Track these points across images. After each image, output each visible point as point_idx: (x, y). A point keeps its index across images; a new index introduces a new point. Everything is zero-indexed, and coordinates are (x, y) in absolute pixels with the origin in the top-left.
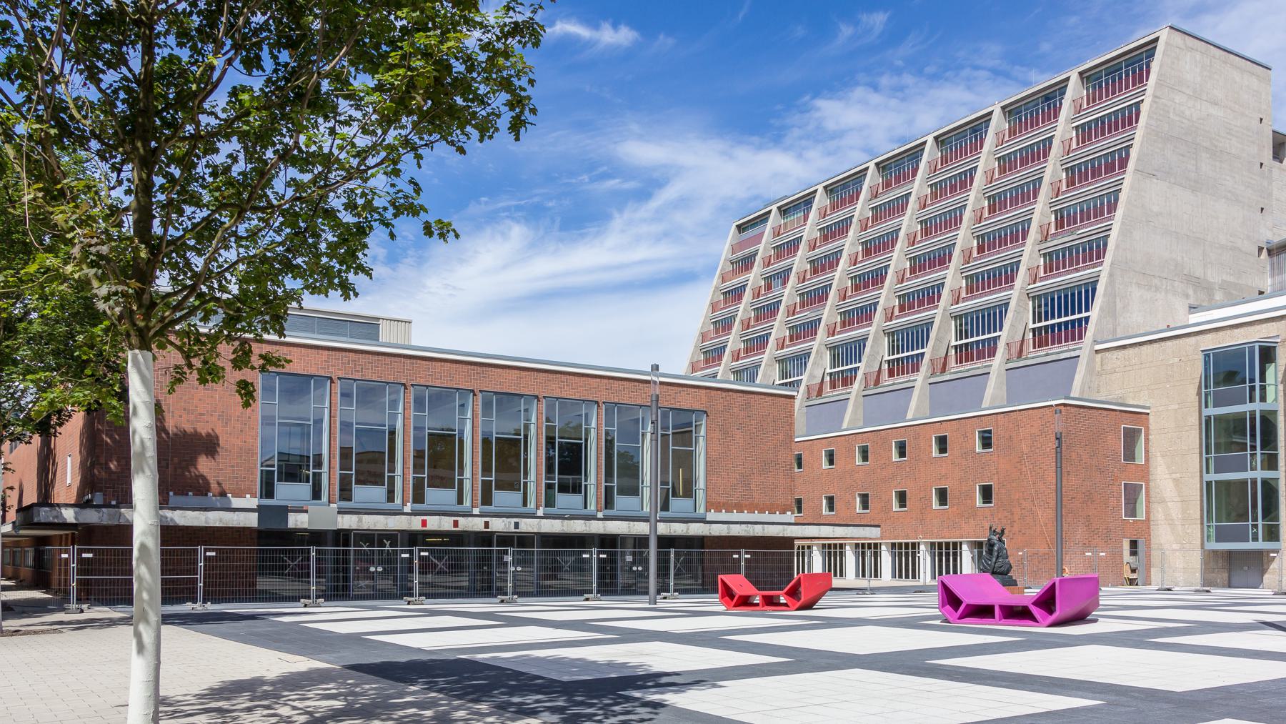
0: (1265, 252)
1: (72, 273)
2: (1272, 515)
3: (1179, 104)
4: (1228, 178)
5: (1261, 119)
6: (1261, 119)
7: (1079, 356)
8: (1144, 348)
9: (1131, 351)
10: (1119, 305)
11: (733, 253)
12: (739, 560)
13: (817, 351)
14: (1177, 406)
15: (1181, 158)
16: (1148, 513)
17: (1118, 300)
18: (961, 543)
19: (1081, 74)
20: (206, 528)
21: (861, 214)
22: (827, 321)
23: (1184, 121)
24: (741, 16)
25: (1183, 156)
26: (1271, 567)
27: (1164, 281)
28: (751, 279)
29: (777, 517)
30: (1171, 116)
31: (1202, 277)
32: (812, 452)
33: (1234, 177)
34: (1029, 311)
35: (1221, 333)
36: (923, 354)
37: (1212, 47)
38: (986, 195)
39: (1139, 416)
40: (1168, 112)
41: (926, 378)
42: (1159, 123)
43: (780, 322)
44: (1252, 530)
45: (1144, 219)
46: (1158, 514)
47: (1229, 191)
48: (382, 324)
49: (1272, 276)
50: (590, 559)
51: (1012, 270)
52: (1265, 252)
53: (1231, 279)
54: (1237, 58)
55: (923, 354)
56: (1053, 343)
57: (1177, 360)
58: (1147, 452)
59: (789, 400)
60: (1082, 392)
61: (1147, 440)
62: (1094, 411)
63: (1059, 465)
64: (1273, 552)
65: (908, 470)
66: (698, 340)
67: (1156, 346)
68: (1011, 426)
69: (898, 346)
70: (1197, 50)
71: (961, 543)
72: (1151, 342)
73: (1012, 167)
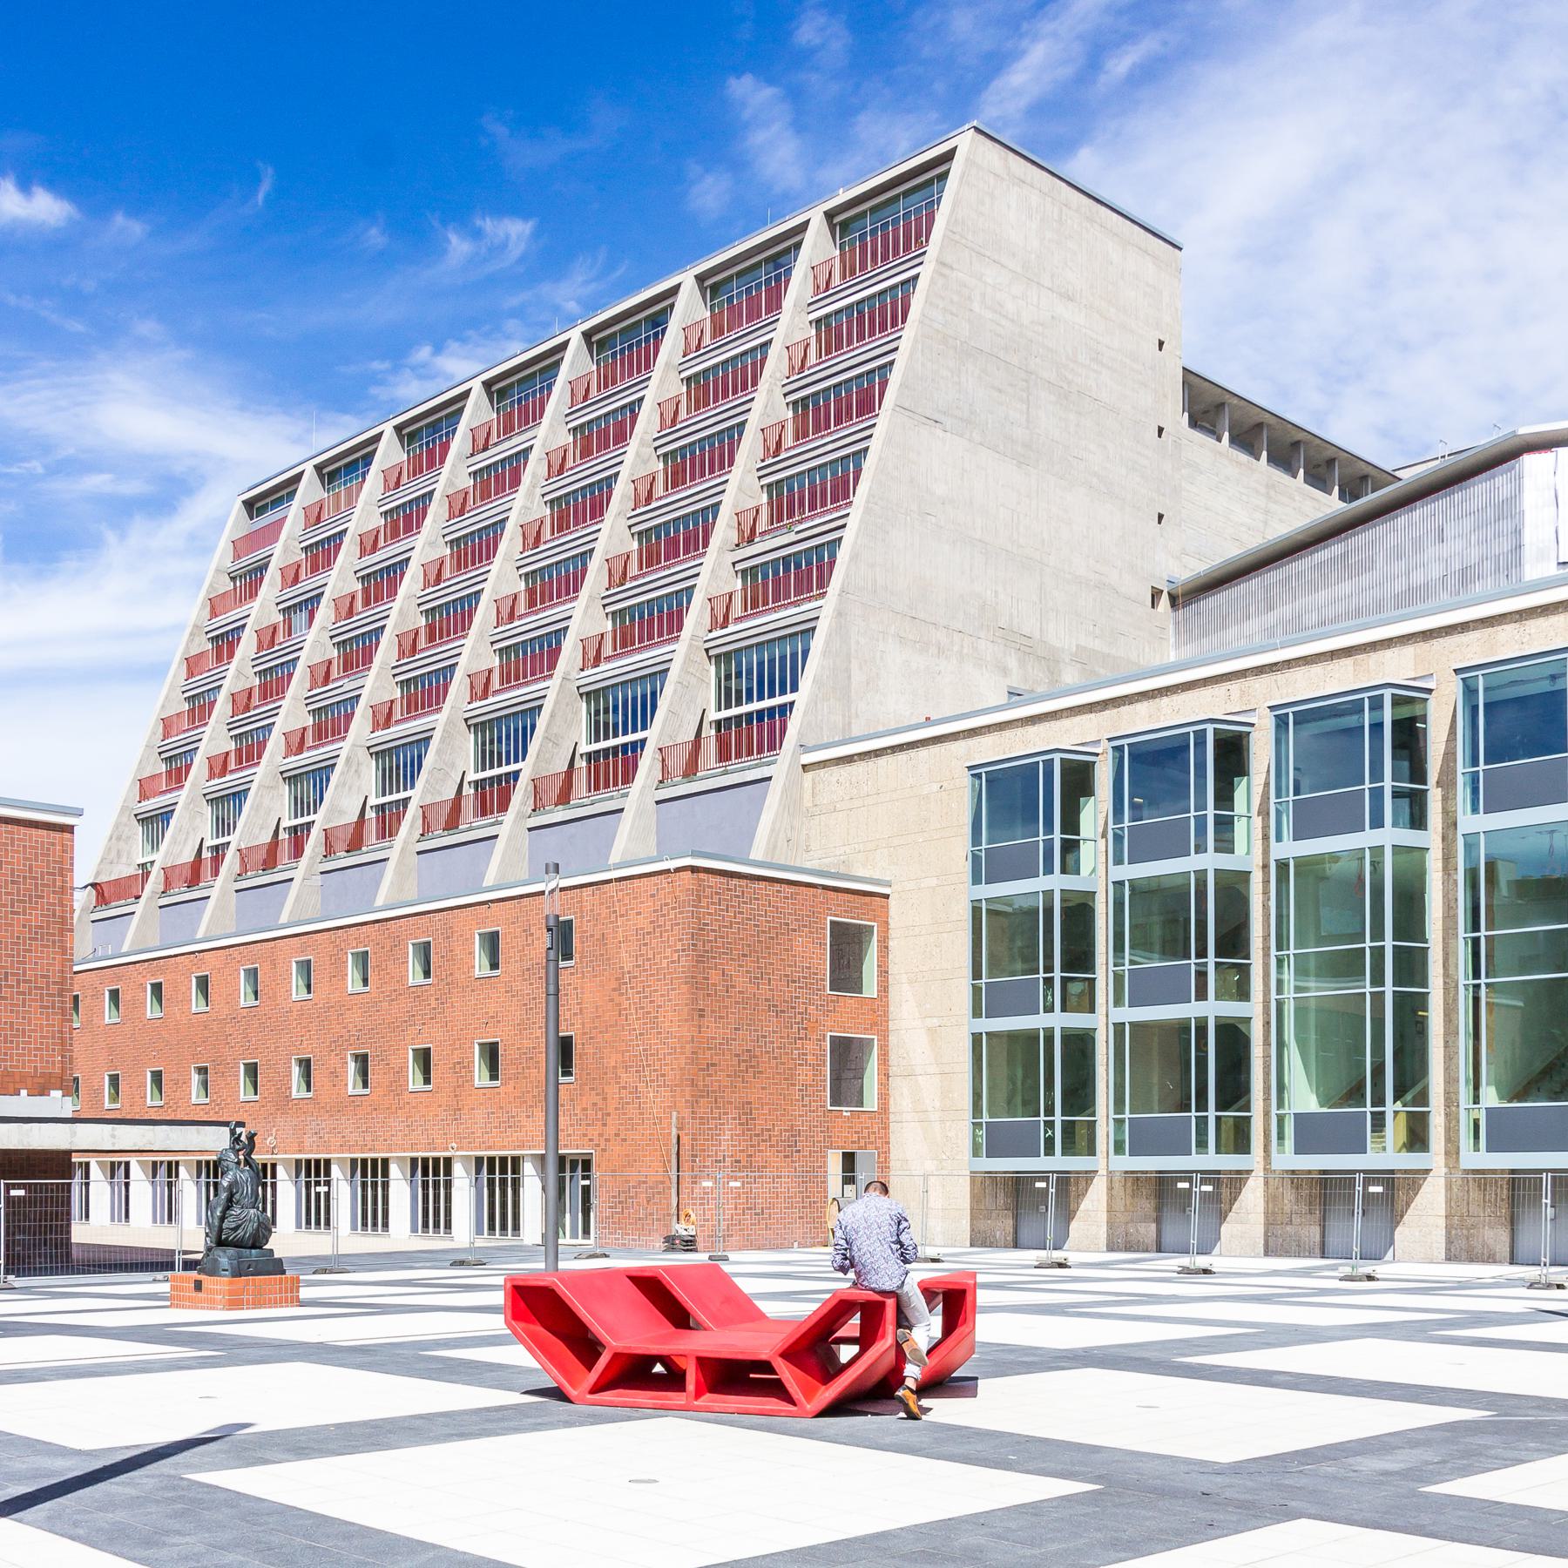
0: (1164, 600)
2: (1242, 1102)
5: (1161, 344)
6: (1161, 344)
7: (769, 779)
8: (882, 761)
9: (859, 768)
10: (857, 677)
11: (237, 556)
13: (348, 760)
14: (933, 882)
16: (884, 1097)
17: (854, 665)
18: (177, 1163)
19: (829, 215)
21: (450, 483)
22: (369, 700)
23: (1003, 322)
25: (1000, 391)
26: (1082, 1207)
27: (957, 637)
28: (254, 613)
30: (976, 307)
31: (1037, 635)
32: (274, 964)
34: (708, 684)
35: (1007, 733)
36: (516, 774)
37: (1064, 185)
38: (660, 451)
41: (520, 816)
43: (294, 698)
44: (1046, 1132)
46: (901, 1100)
49: (1178, 646)
51: (680, 604)
52: (1165, 598)
53: (1097, 645)
54: (1115, 215)
55: (516, 774)
56: (738, 755)
57: (936, 787)
58: (884, 972)
59: (58, 835)
60: (772, 847)
61: (884, 948)
62: (762, 885)
63: (552, 989)
64: (1041, 1179)
65: (433, 1003)
66: (154, 733)
67: (902, 757)
68: (605, 912)
69: (500, 754)
71: (177, 1163)
72: (895, 749)
73: (821, 425)
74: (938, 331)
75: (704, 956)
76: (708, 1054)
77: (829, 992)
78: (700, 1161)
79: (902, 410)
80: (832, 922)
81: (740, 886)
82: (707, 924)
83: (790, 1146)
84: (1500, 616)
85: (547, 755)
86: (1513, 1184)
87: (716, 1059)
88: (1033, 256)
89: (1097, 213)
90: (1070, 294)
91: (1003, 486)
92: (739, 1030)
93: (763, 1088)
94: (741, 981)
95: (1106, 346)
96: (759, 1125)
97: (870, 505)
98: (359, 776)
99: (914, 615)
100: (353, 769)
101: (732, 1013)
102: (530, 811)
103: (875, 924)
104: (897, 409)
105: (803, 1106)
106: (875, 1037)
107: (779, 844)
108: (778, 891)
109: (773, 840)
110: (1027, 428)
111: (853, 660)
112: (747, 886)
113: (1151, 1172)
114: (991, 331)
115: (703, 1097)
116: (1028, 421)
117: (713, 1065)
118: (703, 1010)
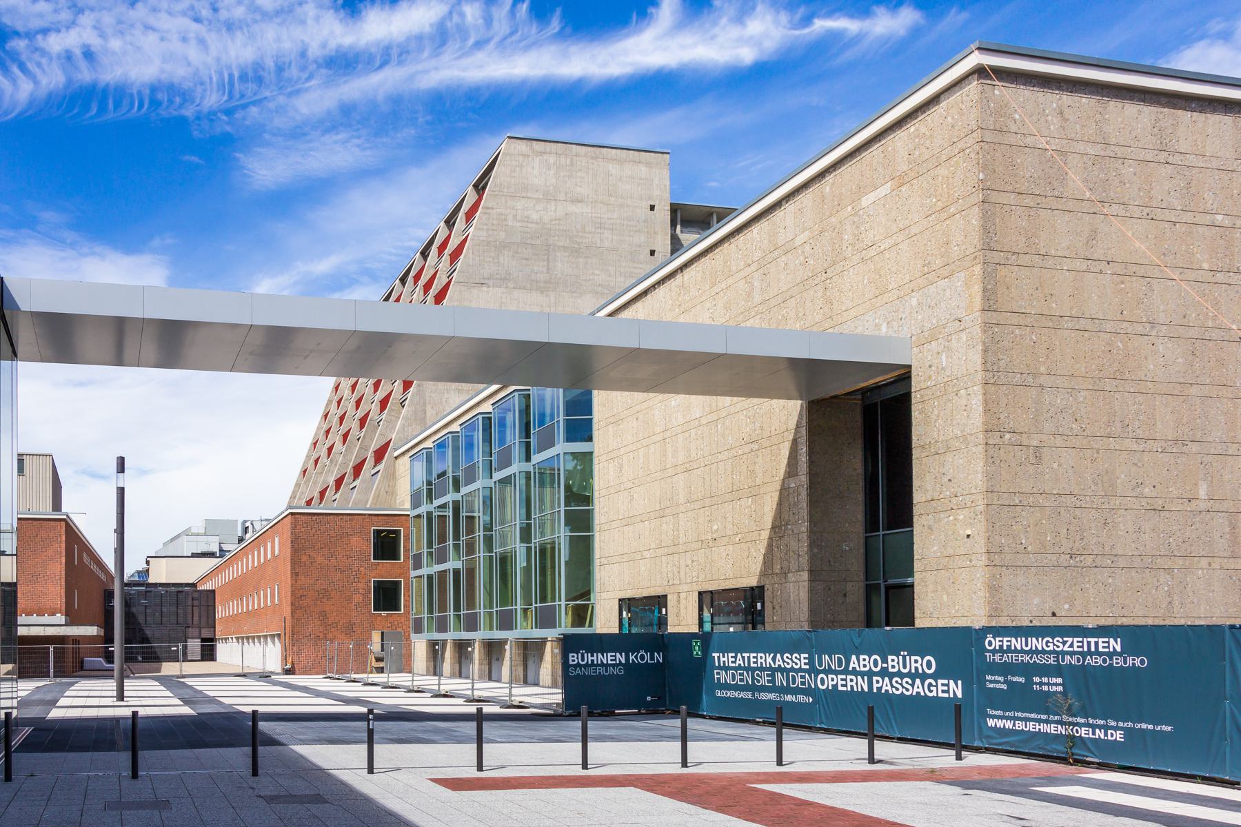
1: (931, 384)
4: (597, 272)
12: (178, 651)
15: (524, 262)
17: (428, 408)
20: (28, 636)
25: (527, 259)
29: (46, 619)
39: (397, 518)
40: (506, 220)
42: (491, 232)
48: (119, 486)
50: (178, 651)
70: (550, 153)
74: (483, 241)
83: (349, 630)
87: (305, 593)
90: (579, 199)
94: (320, 559)
95: (608, 219)
107: (382, 493)
109: (377, 493)
116: (548, 269)
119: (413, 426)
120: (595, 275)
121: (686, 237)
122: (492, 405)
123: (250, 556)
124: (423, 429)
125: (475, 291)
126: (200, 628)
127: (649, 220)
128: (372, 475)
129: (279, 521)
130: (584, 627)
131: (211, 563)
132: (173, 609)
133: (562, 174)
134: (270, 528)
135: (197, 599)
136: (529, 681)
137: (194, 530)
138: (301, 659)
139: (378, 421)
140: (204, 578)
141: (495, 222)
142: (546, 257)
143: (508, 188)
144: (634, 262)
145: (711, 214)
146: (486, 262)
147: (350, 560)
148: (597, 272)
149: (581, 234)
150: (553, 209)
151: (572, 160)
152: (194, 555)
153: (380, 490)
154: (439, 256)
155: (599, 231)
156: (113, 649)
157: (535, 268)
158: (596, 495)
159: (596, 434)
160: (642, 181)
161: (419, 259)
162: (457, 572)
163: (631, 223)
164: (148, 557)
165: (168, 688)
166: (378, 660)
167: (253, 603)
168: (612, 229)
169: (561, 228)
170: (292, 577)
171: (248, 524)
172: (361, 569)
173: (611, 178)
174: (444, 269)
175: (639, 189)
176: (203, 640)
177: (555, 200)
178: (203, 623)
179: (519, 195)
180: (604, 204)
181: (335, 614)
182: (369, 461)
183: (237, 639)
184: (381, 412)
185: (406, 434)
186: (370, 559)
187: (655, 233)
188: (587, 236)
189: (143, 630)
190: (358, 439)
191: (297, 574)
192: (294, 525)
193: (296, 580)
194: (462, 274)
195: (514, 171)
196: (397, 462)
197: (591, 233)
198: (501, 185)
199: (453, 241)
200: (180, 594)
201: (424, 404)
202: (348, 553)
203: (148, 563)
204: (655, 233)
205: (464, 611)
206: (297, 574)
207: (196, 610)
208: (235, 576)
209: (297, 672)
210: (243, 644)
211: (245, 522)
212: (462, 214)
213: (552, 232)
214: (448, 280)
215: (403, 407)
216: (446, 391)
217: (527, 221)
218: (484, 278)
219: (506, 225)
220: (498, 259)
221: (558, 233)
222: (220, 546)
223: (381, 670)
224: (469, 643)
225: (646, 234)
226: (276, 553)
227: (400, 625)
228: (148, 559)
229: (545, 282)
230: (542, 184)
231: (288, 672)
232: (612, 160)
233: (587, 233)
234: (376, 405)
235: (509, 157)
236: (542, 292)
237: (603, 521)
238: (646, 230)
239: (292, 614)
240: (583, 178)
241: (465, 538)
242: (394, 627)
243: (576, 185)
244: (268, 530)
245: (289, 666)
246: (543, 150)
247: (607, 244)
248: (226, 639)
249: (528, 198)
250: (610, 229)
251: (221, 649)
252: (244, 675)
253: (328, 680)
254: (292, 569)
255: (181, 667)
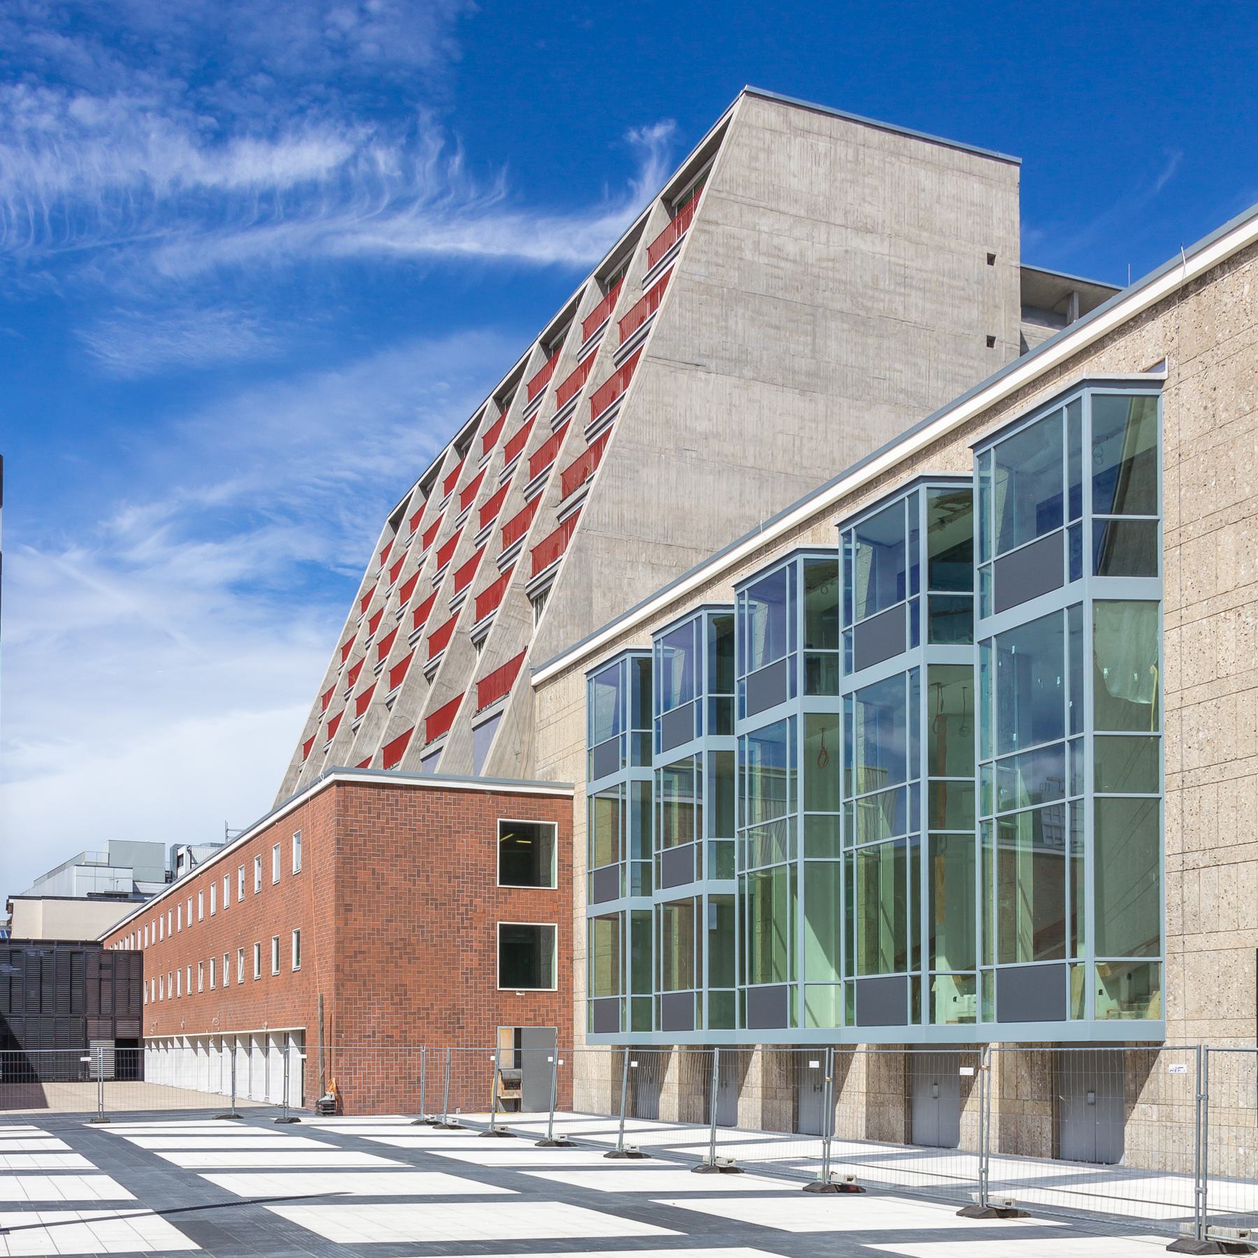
3: (770, 234)
4: (898, 366)
15: (772, 332)
17: (597, 595)
24: (1161, 183)
25: (777, 328)
30: (748, 255)
33: (915, 365)
39: (547, 801)
40: (740, 248)
42: (713, 269)
45: (671, 446)
47: (902, 391)
62: (419, 793)
70: (819, 134)
74: (700, 283)
75: (351, 858)
76: (355, 944)
77: (498, 886)
78: (346, 1037)
79: (655, 360)
80: (500, 822)
81: (393, 796)
82: (356, 831)
83: (452, 1023)
84: (899, 464)
85: (441, 698)
86: (909, 1059)
88: (821, 198)
89: (905, 145)
90: (869, 226)
91: (780, 415)
92: (391, 921)
93: (419, 972)
95: (917, 270)
96: (415, 1004)
97: (616, 449)
98: (379, 728)
99: (669, 542)
100: (374, 723)
101: (383, 907)
102: (423, 744)
103: (557, 823)
104: (650, 359)
105: (467, 987)
106: (556, 925)
108: (437, 799)
109: (498, 754)
110: (813, 358)
111: (594, 589)
112: (401, 796)
113: (786, 1046)
114: (766, 274)
115: (349, 980)
116: (813, 351)
117: (361, 952)
118: (351, 905)
119: (569, 627)
120: (895, 370)
121: (1038, 331)
122: (653, 634)
123: (226, 883)
124: (587, 634)
125: (683, 378)
126: (114, 1020)
127: (986, 281)
128: (474, 729)
129: (306, 801)
130: (1063, 1018)
131: (125, 910)
132: (64, 989)
133: (839, 176)
134: (154, 905)
135: (108, 967)
136: (918, 1134)
137: (90, 858)
138: (355, 1083)
139: (353, 727)
140: (116, 932)
141: (721, 250)
142: (809, 328)
143: (745, 188)
144: (960, 354)
145: (1069, 296)
146: (705, 324)
147: (455, 882)
148: (898, 366)
149: (870, 293)
150: (823, 238)
151: (857, 153)
152: (92, 897)
153: (505, 748)
154: (585, 339)
155: (902, 290)
156: (88, 1059)
157: (792, 346)
158: (1168, 702)
159: (1167, 557)
160: (973, 209)
161: (593, 287)
162: (642, 920)
163: (955, 283)
164: (11, 897)
165: (77, 1147)
166: (511, 1084)
167: (234, 971)
168: (924, 290)
169: (837, 276)
170: (337, 913)
171: (182, 851)
172: (477, 901)
173: (922, 195)
174: (609, 348)
175: (970, 222)
176: (120, 1042)
177: (827, 222)
178: (120, 1010)
179: (763, 204)
180: (910, 241)
181: (423, 991)
182: (467, 702)
183: (193, 1041)
184: (358, 716)
185: (555, 643)
186: (494, 882)
187: (996, 306)
188: (882, 296)
189: (5, 1022)
190: (326, 752)
191: (348, 908)
192: (344, 807)
193: (346, 919)
194: (661, 343)
195: (756, 159)
196: (538, 695)
197: (888, 292)
198: (732, 180)
199: (625, 297)
200: (75, 957)
201: (590, 587)
202: (450, 868)
203: (10, 908)
204: (996, 306)
205: (658, 989)
206: (348, 908)
207: (106, 987)
208: (189, 922)
209: (346, 1109)
210: (234, 1052)
211: (177, 847)
212: (477, 437)
213: (822, 282)
214: (456, 531)
215: (390, 709)
216: (629, 565)
217: (779, 257)
218: (700, 355)
219: (741, 259)
220: (726, 321)
221: (831, 284)
222: (134, 885)
223: (514, 1106)
224: (736, 1058)
225: (981, 307)
226: (200, 918)
227: (551, 1015)
228: (11, 901)
229: (808, 374)
230: (804, 190)
231: (330, 1109)
232: (926, 163)
233: (881, 290)
234: (470, 603)
235: (747, 129)
236: (803, 392)
237: (1194, 759)
238: (980, 299)
239: (337, 989)
240: (876, 188)
241: (662, 850)
242: (539, 1020)
243: (864, 199)
244: (273, 824)
245: (329, 1097)
246: (807, 127)
247: (914, 316)
248: (165, 1041)
249: (780, 212)
250: (920, 289)
251: (155, 1062)
252: (234, 1115)
253: (429, 1130)
254: (338, 898)
255: (101, 1093)
